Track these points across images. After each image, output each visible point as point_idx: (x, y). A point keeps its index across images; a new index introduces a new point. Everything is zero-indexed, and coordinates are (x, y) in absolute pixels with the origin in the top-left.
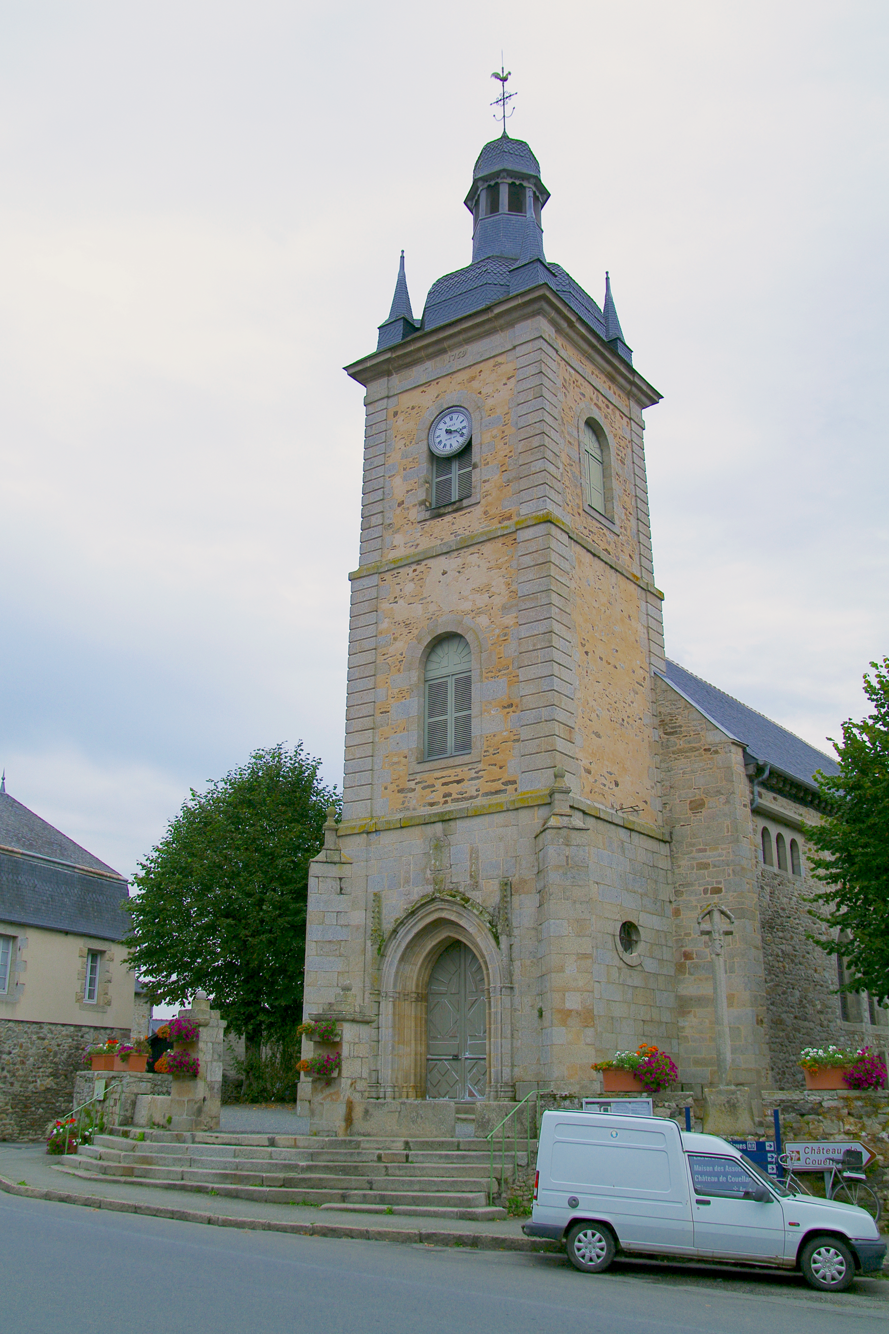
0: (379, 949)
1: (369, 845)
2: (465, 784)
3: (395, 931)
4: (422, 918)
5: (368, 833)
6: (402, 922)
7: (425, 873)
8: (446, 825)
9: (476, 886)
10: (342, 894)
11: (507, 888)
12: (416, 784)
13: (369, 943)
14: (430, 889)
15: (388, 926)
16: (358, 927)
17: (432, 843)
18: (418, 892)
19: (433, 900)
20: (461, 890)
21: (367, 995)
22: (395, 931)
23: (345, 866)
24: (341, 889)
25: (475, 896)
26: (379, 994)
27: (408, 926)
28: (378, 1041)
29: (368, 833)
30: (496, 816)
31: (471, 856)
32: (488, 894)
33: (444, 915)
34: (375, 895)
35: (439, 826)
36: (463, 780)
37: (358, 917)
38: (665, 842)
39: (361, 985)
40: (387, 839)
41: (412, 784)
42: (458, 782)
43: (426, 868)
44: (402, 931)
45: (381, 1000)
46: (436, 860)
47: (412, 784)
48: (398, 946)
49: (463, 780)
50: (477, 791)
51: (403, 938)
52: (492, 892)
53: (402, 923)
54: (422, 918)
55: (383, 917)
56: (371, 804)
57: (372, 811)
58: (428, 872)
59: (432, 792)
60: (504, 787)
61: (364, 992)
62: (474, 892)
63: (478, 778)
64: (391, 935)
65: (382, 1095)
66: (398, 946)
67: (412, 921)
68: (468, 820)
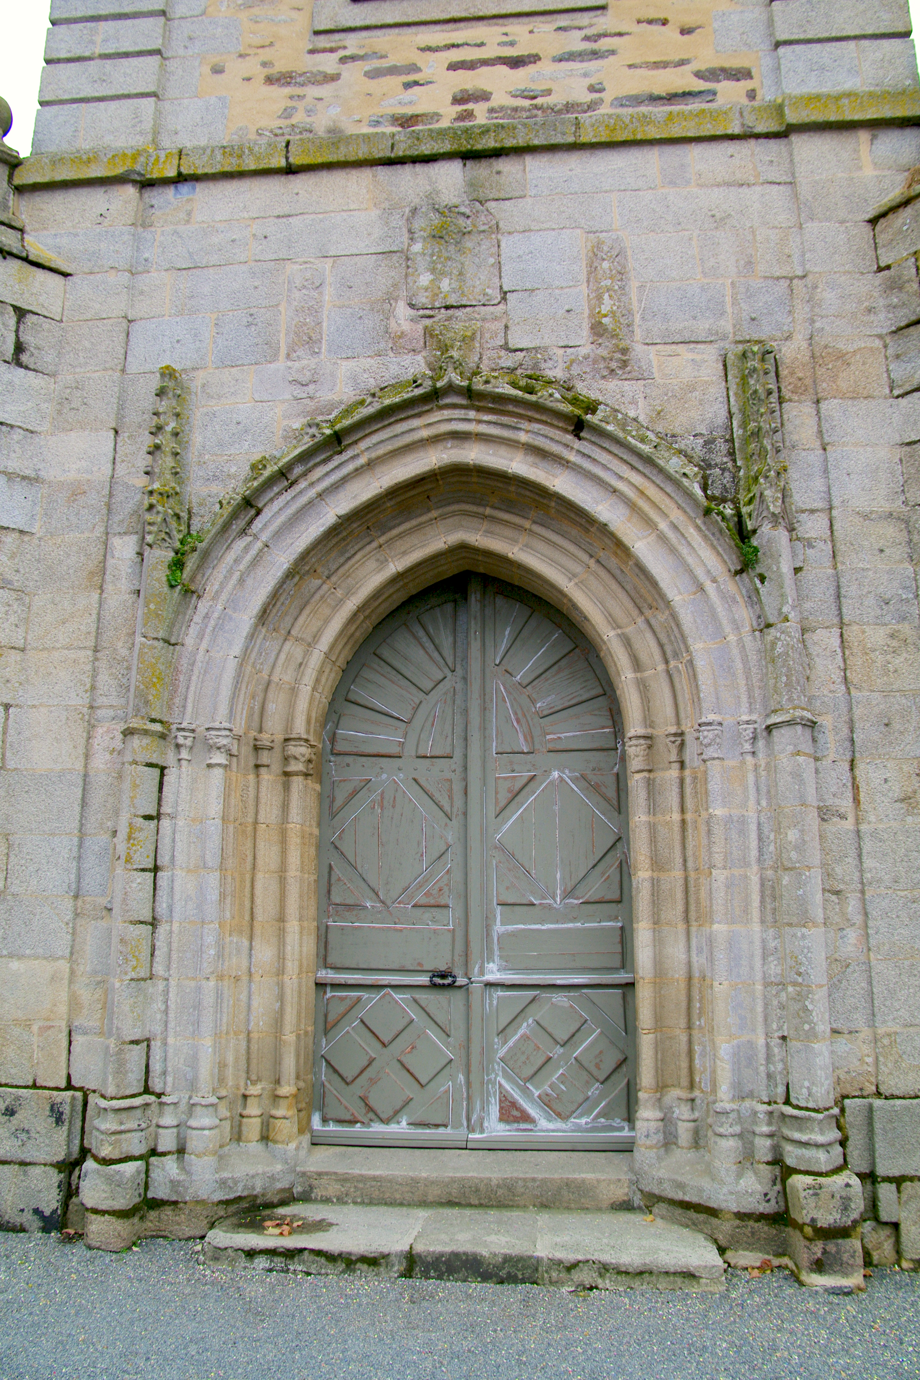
0: (178, 564)
1: (143, 222)
2: (545, 68)
3: (249, 505)
4: (370, 465)
5: (146, 184)
6: (282, 474)
7: (388, 315)
8: (481, 170)
9: (621, 363)
10: (20, 364)
11: (756, 374)
12: (343, 60)
13: (124, 548)
14: (414, 365)
15: (215, 478)
16: (76, 492)
17: (419, 223)
18: (349, 378)
19: (433, 397)
20: (556, 372)
21: (107, 736)
22: (249, 505)
23: (40, 274)
24: (19, 348)
25: (623, 400)
26: (163, 736)
27: (305, 491)
28: (154, 923)
29: (146, 184)
30: (695, 152)
31: (592, 270)
32: (676, 390)
33: (474, 454)
34: (168, 373)
35: (449, 178)
36: (534, 59)
37: (82, 455)
38: (148, 1046)
39: (79, 700)
40: (214, 204)
41: (328, 63)
42: (515, 63)
43: (390, 298)
44: (276, 511)
45: (170, 759)
46: (437, 273)
47: (328, 63)
48: (256, 561)
49: (534, 59)
50: (592, 89)
51: (278, 534)
52: (692, 388)
53: (79, 858)
54: (370, 465)
55: (191, 456)
56: (158, 113)
57: (156, 133)
58: (402, 311)
59: (407, 86)
60: (701, 85)
61: (91, 728)
62: (612, 385)
63: (595, 55)
64: (234, 516)
65: (167, 1142)
66: (256, 561)
67: (323, 475)
68: (574, 163)
